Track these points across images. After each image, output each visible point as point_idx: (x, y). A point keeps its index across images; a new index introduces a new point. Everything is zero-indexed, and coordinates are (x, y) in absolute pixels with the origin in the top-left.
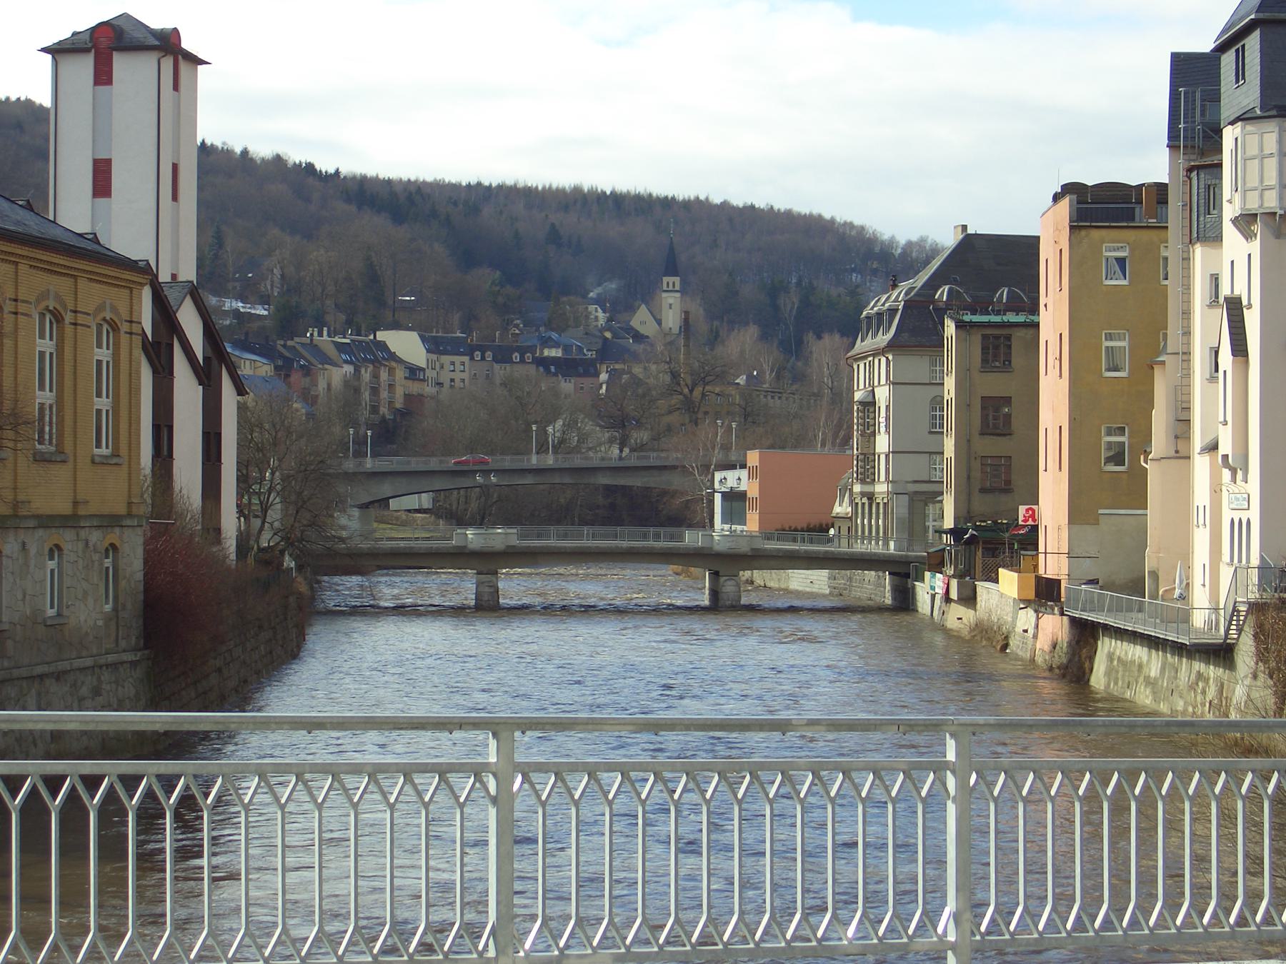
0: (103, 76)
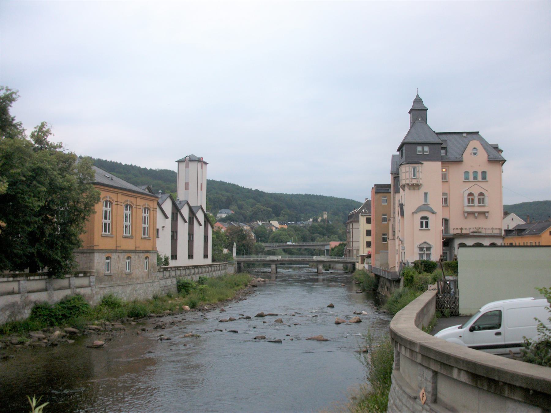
0: (187, 166)
